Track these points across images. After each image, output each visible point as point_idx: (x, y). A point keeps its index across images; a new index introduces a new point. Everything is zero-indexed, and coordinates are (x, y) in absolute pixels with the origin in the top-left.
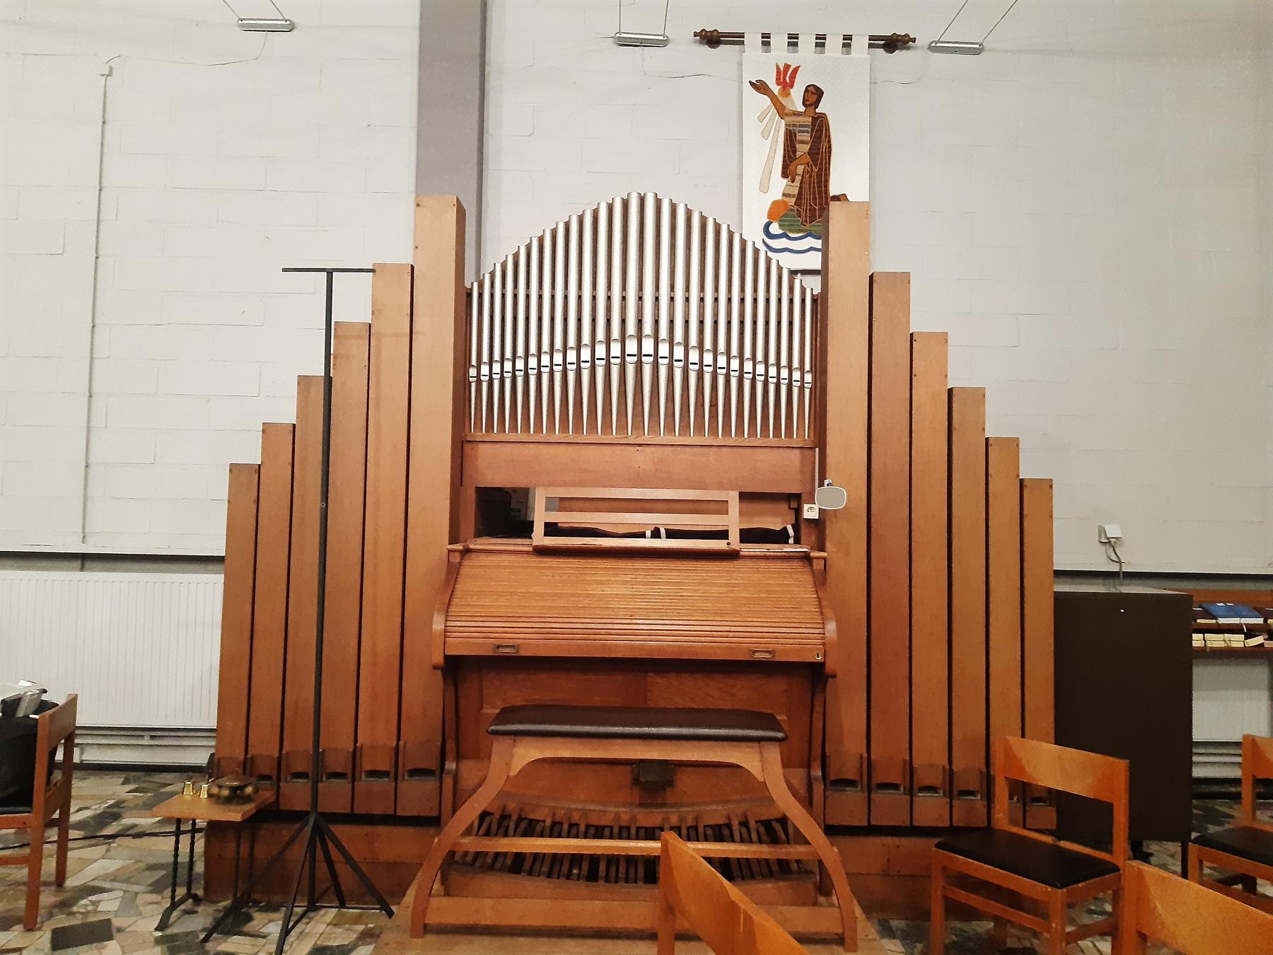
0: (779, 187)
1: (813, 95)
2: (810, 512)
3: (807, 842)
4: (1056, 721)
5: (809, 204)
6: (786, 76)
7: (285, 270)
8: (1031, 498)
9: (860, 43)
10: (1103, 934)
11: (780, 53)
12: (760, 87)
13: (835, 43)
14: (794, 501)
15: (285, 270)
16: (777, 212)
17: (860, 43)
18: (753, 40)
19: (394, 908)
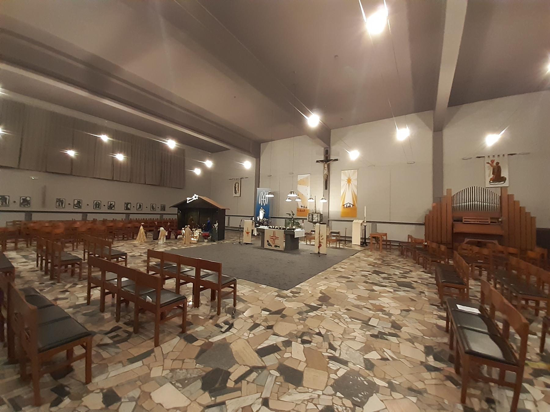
0: (492, 176)
1: (498, 163)
2: (500, 220)
3: (121, 328)
4: (495, 341)
5: (498, 177)
6: (493, 161)
7: (317, 161)
8: (533, 219)
9: (506, 156)
10: (398, 112)
11: (492, 158)
12: (488, 163)
13: (501, 156)
14: (498, 219)
15: (317, 161)
16: (491, 179)
17: (506, 156)
18: (487, 157)
19: (321, 295)
